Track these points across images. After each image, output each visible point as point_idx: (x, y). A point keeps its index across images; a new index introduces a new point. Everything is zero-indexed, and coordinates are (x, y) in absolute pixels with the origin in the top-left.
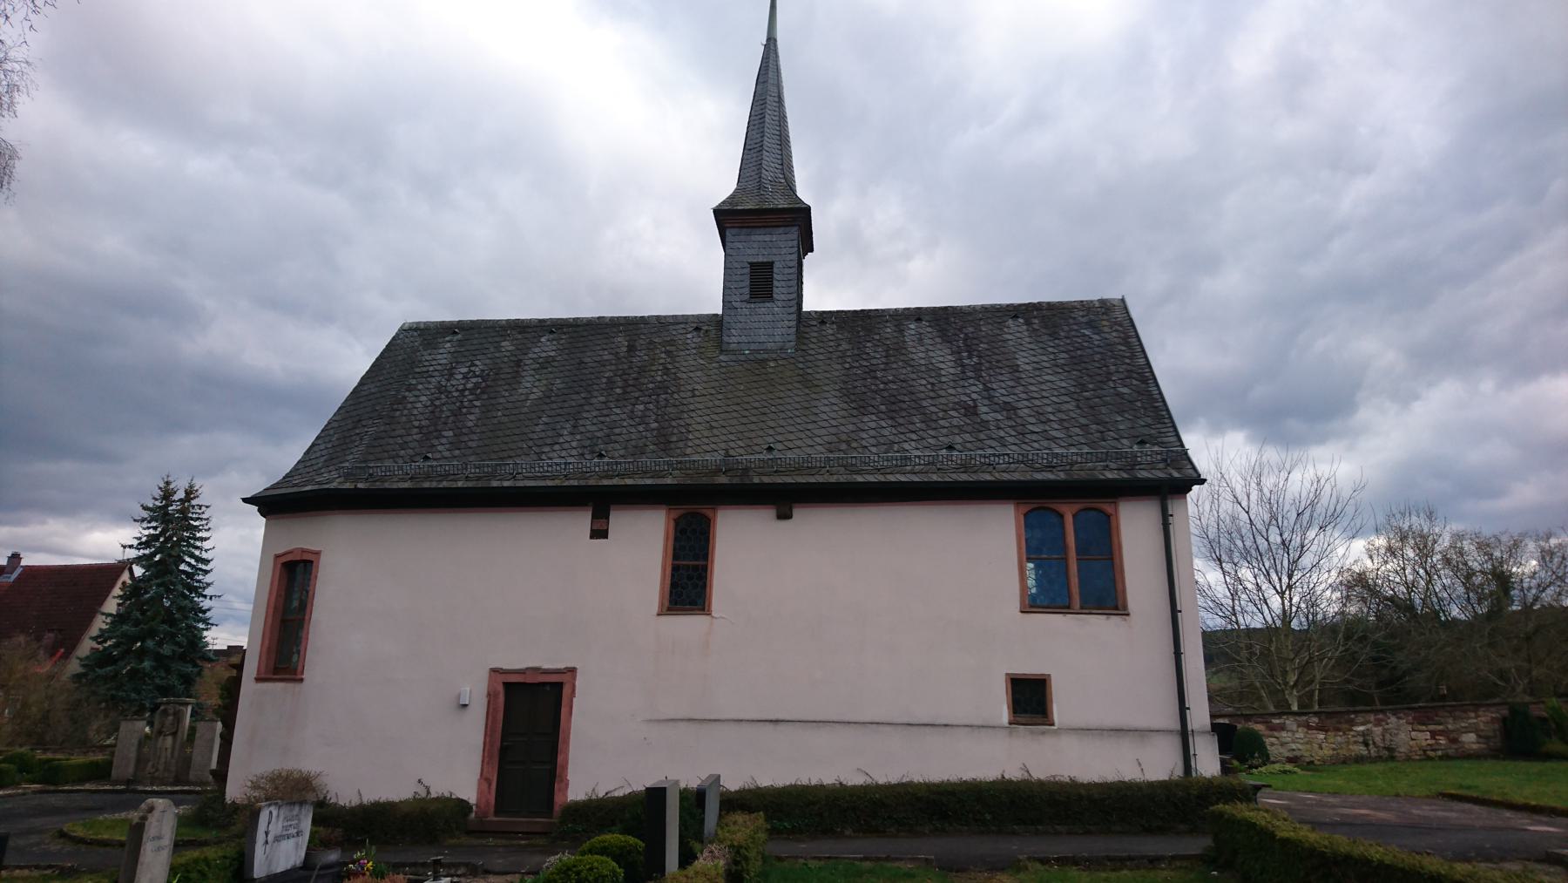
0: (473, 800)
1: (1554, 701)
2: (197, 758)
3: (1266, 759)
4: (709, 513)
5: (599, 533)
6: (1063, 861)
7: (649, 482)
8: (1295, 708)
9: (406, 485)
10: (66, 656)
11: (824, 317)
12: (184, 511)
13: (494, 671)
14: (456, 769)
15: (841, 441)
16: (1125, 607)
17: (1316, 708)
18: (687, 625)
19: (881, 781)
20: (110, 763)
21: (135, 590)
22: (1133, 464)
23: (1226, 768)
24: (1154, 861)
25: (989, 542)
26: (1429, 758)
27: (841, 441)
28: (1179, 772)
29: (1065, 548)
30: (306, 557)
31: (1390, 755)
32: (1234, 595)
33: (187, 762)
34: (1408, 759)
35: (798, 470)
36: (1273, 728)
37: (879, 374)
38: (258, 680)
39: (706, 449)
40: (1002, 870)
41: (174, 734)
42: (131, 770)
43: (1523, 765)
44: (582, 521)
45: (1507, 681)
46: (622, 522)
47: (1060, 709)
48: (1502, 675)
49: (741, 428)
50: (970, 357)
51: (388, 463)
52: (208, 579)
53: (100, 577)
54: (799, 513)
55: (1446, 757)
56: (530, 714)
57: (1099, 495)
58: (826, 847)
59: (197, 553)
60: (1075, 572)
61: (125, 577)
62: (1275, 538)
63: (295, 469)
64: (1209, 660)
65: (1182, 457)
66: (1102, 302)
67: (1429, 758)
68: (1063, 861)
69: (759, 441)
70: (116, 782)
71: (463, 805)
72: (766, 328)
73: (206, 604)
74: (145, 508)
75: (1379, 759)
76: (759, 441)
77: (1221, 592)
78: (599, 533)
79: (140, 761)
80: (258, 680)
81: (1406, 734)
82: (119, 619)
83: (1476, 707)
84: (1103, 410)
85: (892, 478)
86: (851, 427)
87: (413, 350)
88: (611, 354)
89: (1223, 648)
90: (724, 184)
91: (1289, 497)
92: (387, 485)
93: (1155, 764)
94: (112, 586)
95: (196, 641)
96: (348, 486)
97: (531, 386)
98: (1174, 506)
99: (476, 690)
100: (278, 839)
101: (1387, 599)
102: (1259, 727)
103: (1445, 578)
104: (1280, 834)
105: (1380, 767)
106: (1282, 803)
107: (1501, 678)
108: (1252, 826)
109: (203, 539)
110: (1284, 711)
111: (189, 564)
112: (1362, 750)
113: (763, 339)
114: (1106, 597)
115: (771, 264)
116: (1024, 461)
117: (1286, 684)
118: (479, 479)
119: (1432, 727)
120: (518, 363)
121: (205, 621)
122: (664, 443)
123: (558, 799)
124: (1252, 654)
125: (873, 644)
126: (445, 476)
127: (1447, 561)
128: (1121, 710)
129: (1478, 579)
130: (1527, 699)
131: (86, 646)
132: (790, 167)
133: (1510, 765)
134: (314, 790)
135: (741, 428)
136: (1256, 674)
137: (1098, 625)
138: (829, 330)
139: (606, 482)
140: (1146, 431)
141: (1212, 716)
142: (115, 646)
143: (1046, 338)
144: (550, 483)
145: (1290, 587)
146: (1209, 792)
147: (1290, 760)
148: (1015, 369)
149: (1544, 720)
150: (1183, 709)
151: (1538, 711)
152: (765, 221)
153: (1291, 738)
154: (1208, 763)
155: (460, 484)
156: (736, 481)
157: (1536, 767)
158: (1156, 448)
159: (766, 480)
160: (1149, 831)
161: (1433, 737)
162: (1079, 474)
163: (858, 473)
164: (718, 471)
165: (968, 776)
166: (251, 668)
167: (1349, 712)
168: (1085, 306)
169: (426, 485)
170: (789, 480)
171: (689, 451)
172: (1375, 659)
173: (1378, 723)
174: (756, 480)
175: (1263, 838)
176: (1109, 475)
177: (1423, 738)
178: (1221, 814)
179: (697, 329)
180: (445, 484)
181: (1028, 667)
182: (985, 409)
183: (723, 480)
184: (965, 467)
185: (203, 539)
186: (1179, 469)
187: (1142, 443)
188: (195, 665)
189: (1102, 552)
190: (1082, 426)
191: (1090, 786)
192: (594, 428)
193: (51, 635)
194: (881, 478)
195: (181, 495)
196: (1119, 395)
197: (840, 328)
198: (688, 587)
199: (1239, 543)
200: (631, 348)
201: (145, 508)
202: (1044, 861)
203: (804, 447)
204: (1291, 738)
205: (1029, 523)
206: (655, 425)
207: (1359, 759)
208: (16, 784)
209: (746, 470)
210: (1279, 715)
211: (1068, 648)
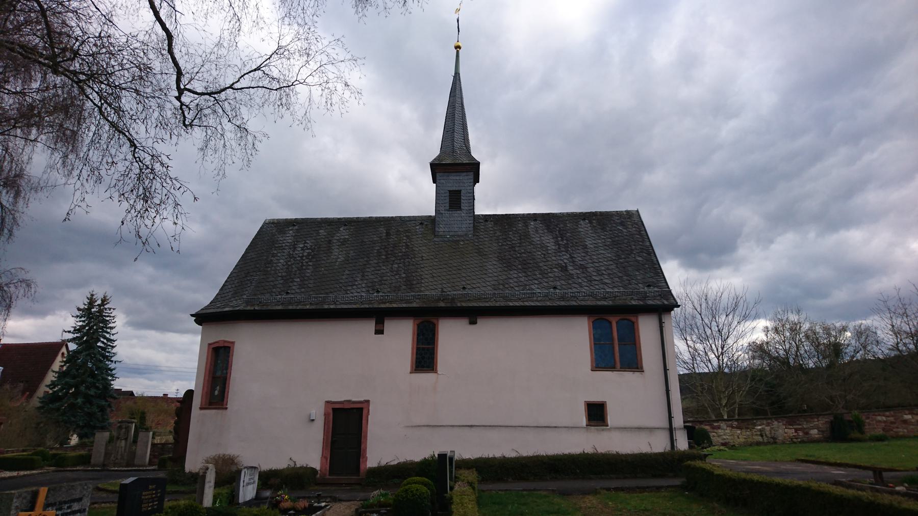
0: (318, 468)
1: (856, 412)
2: (139, 452)
3: (711, 444)
4: (435, 321)
6: (617, 489)
7: (404, 305)
8: (726, 417)
9: (280, 308)
10: (31, 396)
11: (487, 218)
12: (100, 311)
13: (327, 402)
14: (310, 453)
15: (499, 284)
16: (642, 368)
17: (737, 417)
18: (425, 378)
19: (525, 454)
20: (90, 456)
21: (72, 357)
22: (645, 297)
23: (690, 446)
24: (658, 489)
25: (574, 338)
26: (795, 443)
27: (499, 284)
28: (668, 448)
29: (612, 339)
30: (226, 345)
31: (774, 441)
32: (693, 358)
33: (133, 454)
34: (784, 443)
35: (479, 299)
36: (714, 428)
37: (517, 249)
38: (201, 408)
39: (431, 289)
40: (589, 494)
41: (126, 439)
42: (102, 459)
43: (839, 445)
44: (369, 326)
45: (834, 402)
46: (390, 326)
47: (612, 418)
48: (831, 398)
49: (448, 277)
50: (562, 240)
51: (267, 296)
52: (114, 350)
53: (48, 351)
54: (480, 321)
55: (802, 442)
56: (346, 424)
57: (629, 312)
58: (502, 486)
59: (108, 336)
60: (616, 350)
61: (64, 350)
62: (715, 329)
63: (216, 298)
64: (683, 391)
65: (667, 293)
66: (627, 212)
67: (795, 443)
68: (617, 489)
69: (458, 284)
70: (94, 466)
71: (313, 470)
72: (457, 224)
73: (112, 366)
74: (79, 309)
75: (768, 443)
76: (458, 284)
77: (687, 356)
78: (379, 331)
79: (107, 454)
80: (201, 408)
81: (782, 430)
82: (62, 375)
83: (818, 416)
84: (630, 269)
85: (527, 304)
86: (504, 277)
87: (273, 235)
88: (377, 238)
89: (689, 383)
90: (434, 151)
91: (722, 306)
92: (270, 308)
93: (658, 444)
94: (56, 355)
95: (107, 385)
96: (249, 308)
97: (338, 255)
98: (665, 319)
99: (318, 412)
100: (248, 484)
101: (774, 358)
102: (707, 427)
103: (807, 346)
104: (716, 473)
105: (769, 447)
106: (719, 462)
107: (832, 400)
108: (704, 470)
109: (112, 328)
110: (720, 419)
111: (103, 342)
112: (760, 439)
113: (456, 229)
114: (633, 363)
115: (460, 191)
116: (592, 295)
117: (721, 405)
118: (317, 304)
120: (330, 242)
121: (112, 376)
122: (410, 286)
123: (362, 467)
124: (703, 389)
125: (514, 387)
126: (299, 303)
127: (807, 337)
128: (641, 417)
129: (822, 347)
130: (845, 411)
131: (43, 389)
132: (468, 140)
133: (833, 445)
134: (236, 464)
135: (448, 277)
136: (707, 395)
137: (629, 377)
138: (490, 225)
139: (383, 306)
140: (651, 280)
141: (684, 422)
142: (61, 390)
143: (599, 231)
144: (354, 306)
145: (722, 354)
146: (683, 457)
147: (723, 444)
148: (585, 247)
149: (850, 422)
150: (670, 417)
151: (848, 417)
152: (455, 168)
153: (723, 433)
154: (682, 443)
155: (308, 307)
156: (449, 305)
157: (844, 445)
158: (656, 289)
159: (464, 304)
160: (654, 476)
161: (796, 432)
162: (619, 302)
163: (510, 300)
164: (439, 300)
165: (567, 452)
166: (197, 401)
167: (753, 419)
168: (619, 214)
169: (290, 307)
170: (475, 304)
171: (423, 289)
172: (767, 391)
173: (768, 425)
174: (459, 305)
175: (709, 474)
176: (634, 303)
177: (791, 432)
178: (689, 466)
179: (421, 224)
180: (299, 307)
181: (595, 398)
182: (571, 268)
183: (442, 304)
184: (563, 298)
185: (112, 328)
186: (667, 300)
187: (649, 286)
188: (107, 401)
189: (631, 341)
190: (619, 277)
191: (627, 455)
192: (372, 277)
193: (22, 384)
194: (522, 304)
195: (99, 302)
196: (637, 261)
197: (495, 224)
198: (425, 359)
199: (696, 330)
200: (388, 234)
201: (79, 309)
202: (608, 489)
203: (482, 286)
204: (723, 433)
205: (595, 326)
206: (404, 275)
207: (758, 444)
208: (41, 468)
209: (453, 299)
210: (717, 421)
211: (613, 387)
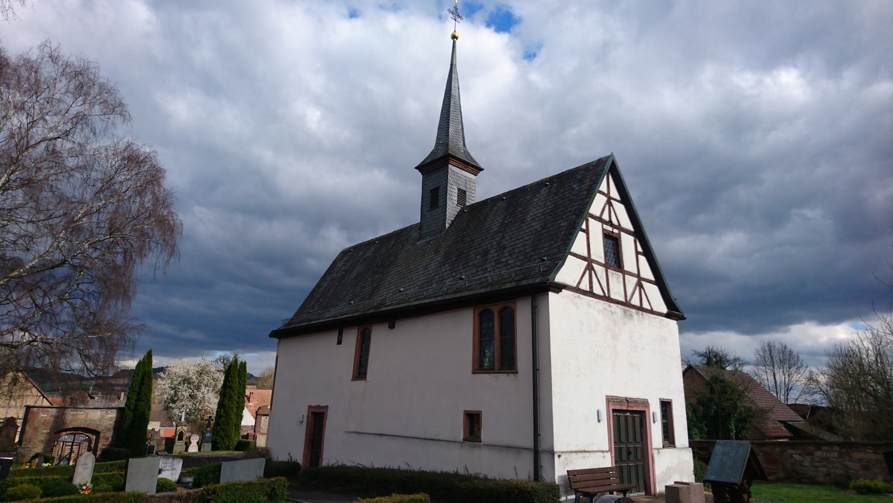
5: (339, 342)
18: (360, 383)
44: (334, 337)
47: (487, 433)
114: (508, 364)
137: (504, 380)
181: (472, 408)
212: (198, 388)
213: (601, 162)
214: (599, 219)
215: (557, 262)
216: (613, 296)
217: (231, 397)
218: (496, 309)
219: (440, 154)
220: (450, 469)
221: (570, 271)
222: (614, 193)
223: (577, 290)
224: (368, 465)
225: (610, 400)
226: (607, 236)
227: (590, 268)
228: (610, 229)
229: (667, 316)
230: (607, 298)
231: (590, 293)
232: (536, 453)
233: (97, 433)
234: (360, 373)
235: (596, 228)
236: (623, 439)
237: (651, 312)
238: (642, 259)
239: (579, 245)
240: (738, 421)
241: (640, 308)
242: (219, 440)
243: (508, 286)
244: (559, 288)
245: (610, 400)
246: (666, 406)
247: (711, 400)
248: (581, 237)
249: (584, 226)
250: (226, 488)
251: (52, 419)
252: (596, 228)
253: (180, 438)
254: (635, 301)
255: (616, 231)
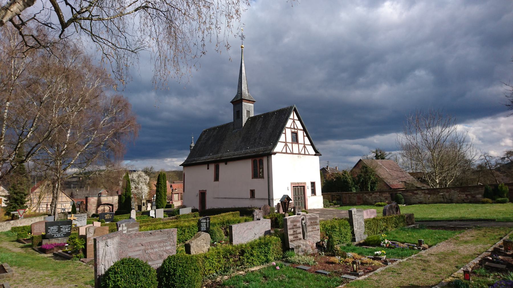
5: (208, 169)
18: (217, 182)
44: (206, 166)
47: (256, 196)
54: (228, 163)
119: (466, 193)
181: (252, 189)
189: (261, 163)
212: (138, 184)
213: (291, 108)
214: (290, 128)
215: (275, 145)
216: (294, 152)
217: (161, 188)
218: (258, 159)
219: (239, 98)
220: (247, 206)
221: (279, 147)
222: (296, 118)
223: (282, 153)
224: (222, 207)
225: (291, 184)
226: (292, 133)
227: (286, 145)
228: (294, 130)
229: (315, 155)
230: (292, 153)
231: (286, 153)
232: (269, 200)
233: (112, 205)
234: (217, 178)
235: (288, 132)
236: (297, 194)
237: (309, 155)
238: (306, 138)
239: (282, 138)
240: (372, 183)
241: (305, 154)
242: (159, 205)
243: (261, 153)
244: (275, 154)
245: (291, 184)
246: (313, 184)
247: (360, 175)
248: (283, 136)
249: (284, 132)
250: (183, 215)
251: (96, 201)
252: (288, 132)
253: (144, 205)
254: (303, 152)
255: (296, 131)
